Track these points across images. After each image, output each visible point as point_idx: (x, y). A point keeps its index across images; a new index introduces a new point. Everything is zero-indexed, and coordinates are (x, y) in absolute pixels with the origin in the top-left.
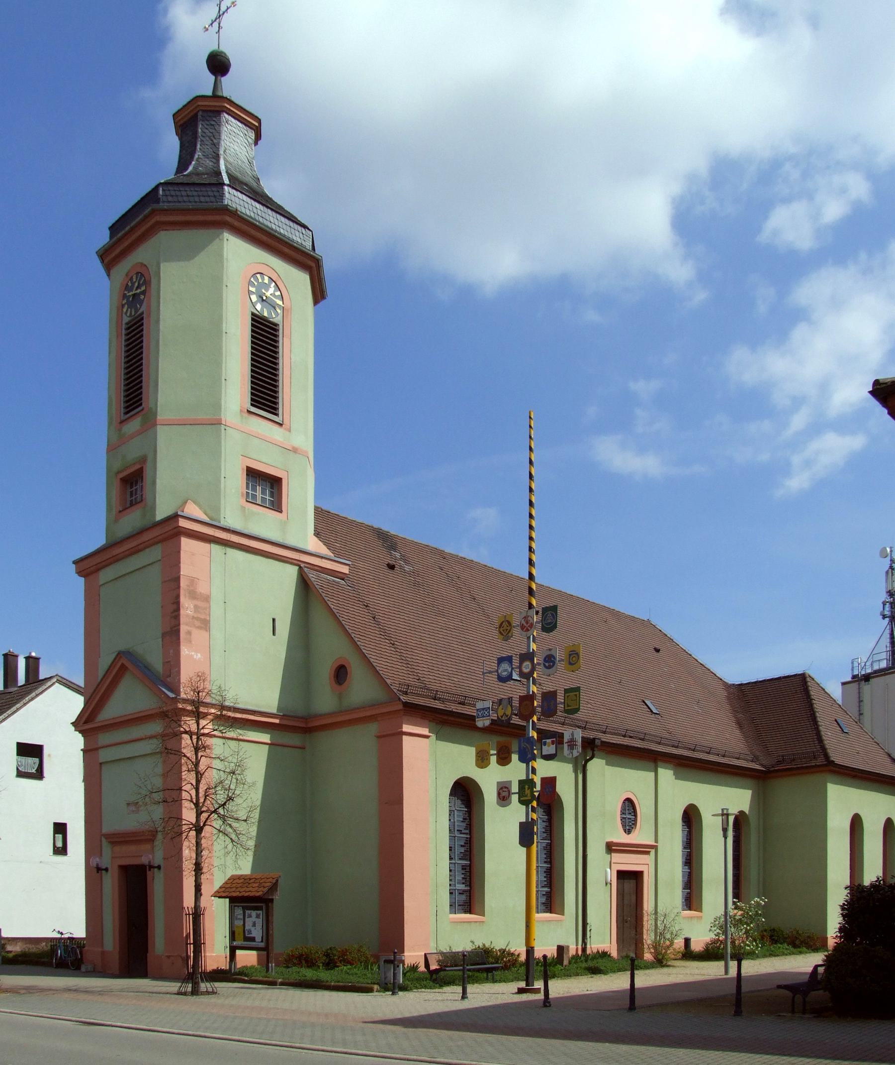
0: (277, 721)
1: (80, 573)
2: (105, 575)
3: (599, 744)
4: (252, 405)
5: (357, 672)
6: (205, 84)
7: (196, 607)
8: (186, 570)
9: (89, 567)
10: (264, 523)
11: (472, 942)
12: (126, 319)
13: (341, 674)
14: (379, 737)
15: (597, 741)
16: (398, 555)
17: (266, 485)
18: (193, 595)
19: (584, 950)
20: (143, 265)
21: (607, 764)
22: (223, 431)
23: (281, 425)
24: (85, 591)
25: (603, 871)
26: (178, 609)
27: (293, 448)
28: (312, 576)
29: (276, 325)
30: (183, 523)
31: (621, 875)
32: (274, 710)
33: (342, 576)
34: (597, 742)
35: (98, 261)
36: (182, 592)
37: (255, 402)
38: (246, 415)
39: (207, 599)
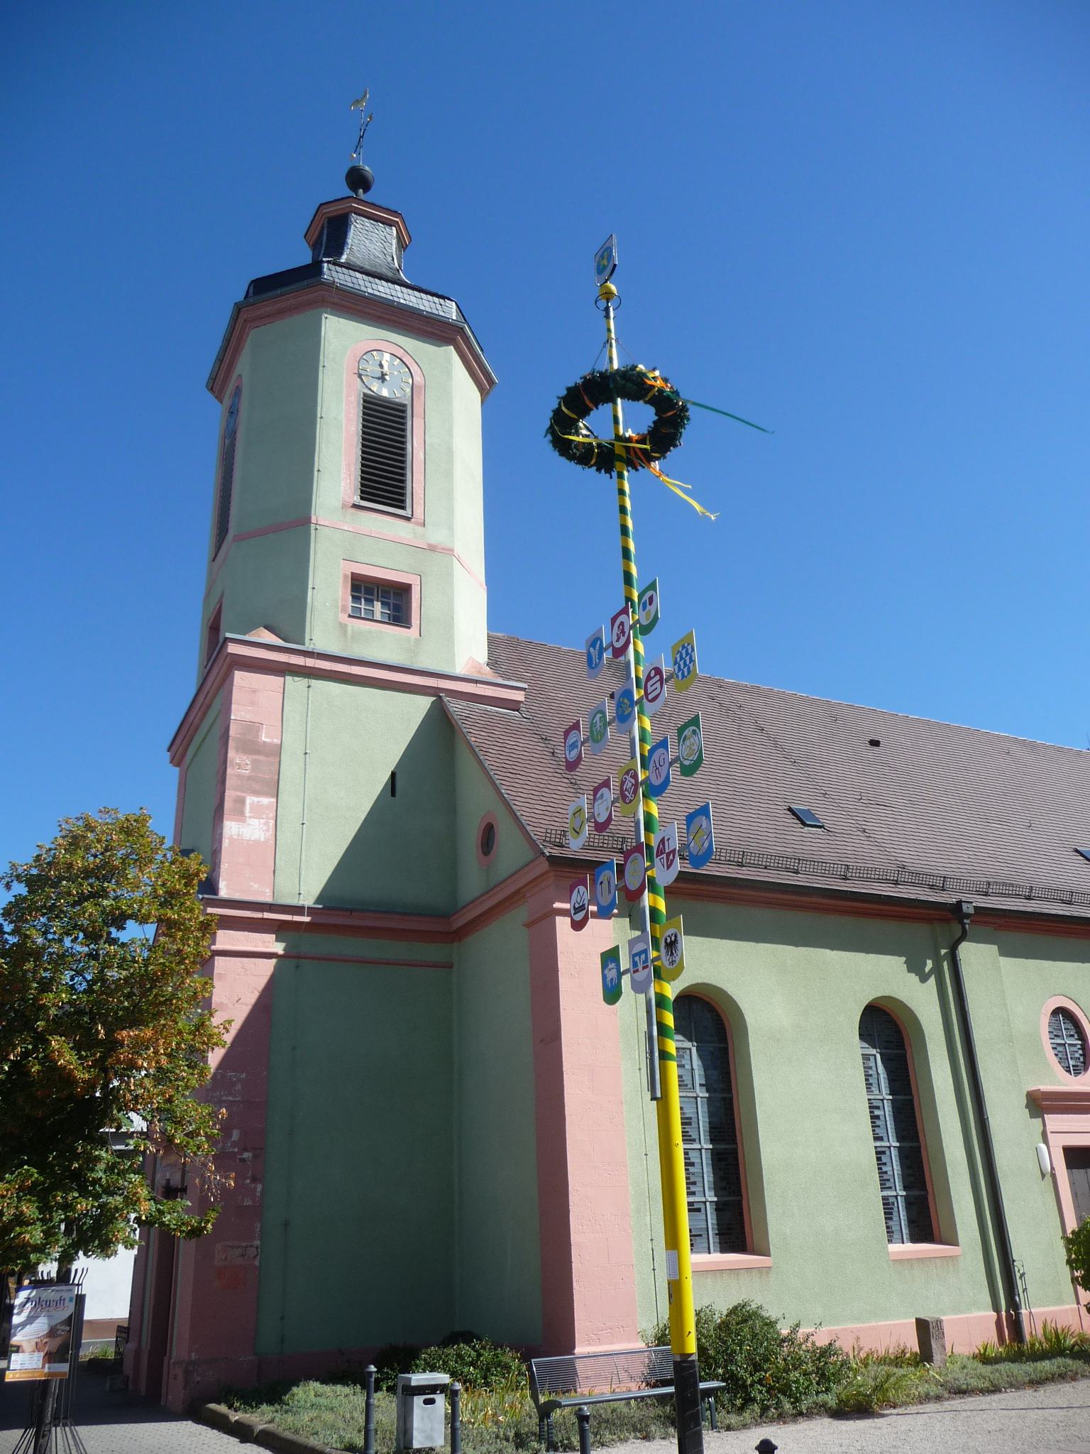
0: (307, 919)
3: (972, 911)
4: (362, 498)
7: (254, 762)
8: (239, 712)
10: (381, 642)
11: (923, 1327)
13: (488, 837)
15: (964, 906)
17: (388, 598)
18: (252, 747)
19: (368, 1397)
21: (1003, 953)
22: (313, 532)
23: (408, 519)
24: (365, 820)
27: (430, 545)
29: (405, 406)
30: (232, 649)
33: (514, 705)
35: (209, 394)
36: (231, 743)
38: (353, 510)
39: (276, 751)
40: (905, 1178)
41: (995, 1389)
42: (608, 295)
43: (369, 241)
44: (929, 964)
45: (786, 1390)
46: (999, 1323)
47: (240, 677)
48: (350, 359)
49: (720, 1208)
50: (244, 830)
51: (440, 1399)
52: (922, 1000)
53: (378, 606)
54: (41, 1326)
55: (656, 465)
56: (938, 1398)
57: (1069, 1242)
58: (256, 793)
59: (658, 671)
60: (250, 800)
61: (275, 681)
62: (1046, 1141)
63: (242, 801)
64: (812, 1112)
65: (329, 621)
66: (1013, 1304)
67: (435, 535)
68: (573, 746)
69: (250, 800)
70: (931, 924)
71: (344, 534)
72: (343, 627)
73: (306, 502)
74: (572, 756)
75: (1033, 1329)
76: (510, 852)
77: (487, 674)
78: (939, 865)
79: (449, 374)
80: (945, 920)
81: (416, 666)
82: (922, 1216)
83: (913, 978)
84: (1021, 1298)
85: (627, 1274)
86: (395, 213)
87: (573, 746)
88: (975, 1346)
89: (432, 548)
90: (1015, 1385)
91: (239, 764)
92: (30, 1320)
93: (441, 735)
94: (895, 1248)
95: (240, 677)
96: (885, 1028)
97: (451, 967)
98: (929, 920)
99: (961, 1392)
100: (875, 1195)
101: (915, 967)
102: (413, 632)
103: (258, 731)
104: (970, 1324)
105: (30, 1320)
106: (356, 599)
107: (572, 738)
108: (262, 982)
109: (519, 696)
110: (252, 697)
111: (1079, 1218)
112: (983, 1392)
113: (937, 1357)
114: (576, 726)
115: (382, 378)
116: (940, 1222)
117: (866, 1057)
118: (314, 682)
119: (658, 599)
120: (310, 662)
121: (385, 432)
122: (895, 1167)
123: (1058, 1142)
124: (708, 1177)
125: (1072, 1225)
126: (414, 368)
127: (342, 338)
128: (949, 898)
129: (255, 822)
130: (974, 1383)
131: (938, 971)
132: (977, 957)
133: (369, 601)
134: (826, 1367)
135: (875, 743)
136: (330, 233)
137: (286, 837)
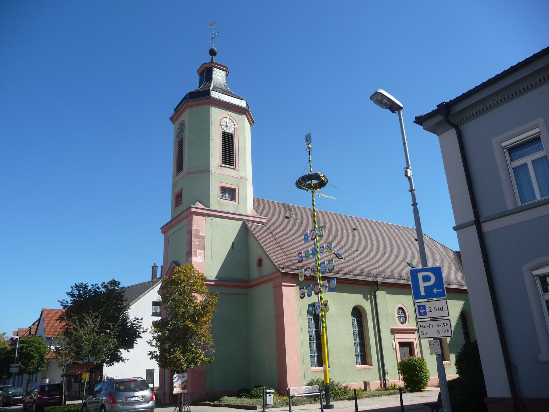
0: (214, 283)
1: (162, 232)
2: (170, 232)
5: (265, 262)
6: (208, 59)
8: (194, 227)
9: (165, 229)
10: (229, 206)
11: (365, 383)
12: (178, 139)
13: (260, 263)
14: (274, 288)
16: (291, 213)
17: (230, 193)
18: (198, 237)
20: (183, 121)
21: (387, 293)
25: (391, 343)
26: (191, 243)
28: (249, 224)
30: (193, 210)
31: (402, 345)
32: (213, 278)
33: (263, 223)
34: (379, 283)
36: (193, 236)
37: (224, 162)
39: (204, 238)
40: (360, 349)
41: (381, 396)
42: (309, 148)
43: (219, 76)
44: (369, 296)
45: (338, 395)
46: (381, 384)
47: (195, 218)
48: (220, 121)
49: (318, 357)
50: (197, 260)
51: (272, 395)
52: (367, 306)
53: (227, 194)
54: (180, 382)
55: (318, 190)
56: (369, 397)
57: (398, 364)
58: (200, 249)
59: (323, 247)
60: (198, 251)
61: (203, 218)
62: (394, 341)
63: (196, 252)
64: (340, 332)
65: (217, 201)
66: (385, 379)
67: (242, 174)
68: (300, 257)
69: (198, 251)
70: (370, 287)
71: (219, 175)
72: (219, 202)
73: (208, 165)
74: (300, 259)
75: (389, 385)
76: (267, 269)
77: (255, 214)
78: (372, 269)
79: (244, 124)
80: (373, 285)
81: (238, 213)
82: (364, 359)
83: (365, 300)
84: (386, 378)
85: (300, 372)
86: (225, 67)
87: (300, 257)
88: (376, 388)
89: (241, 178)
90: (386, 395)
91: (195, 241)
92: (178, 380)
93: (245, 231)
94: (358, 366)
95: (195, 218)
96: (358, 313)
97: (248, 295)
98: (369, 285)
99: (374, 396)
100: (354, 353)
101: (365, 297)
102: (236, 203)
103: (199, 232)
104: (375, 384)
105: (178, 380)
106: (221, 193)
107: (300, 255)
108: (455, 378)
109: (264, 221)
110: (198, 223)
111: (401, 359)
112: (378, 396)
113: (368, 390)
114: (301, 253)
115: (227, 126)
116: (368, 360)
117: (353, 320)
118: (213, 218)
119: (323, 230)
120: (212, 213)
121: (228, 140)
122: (358, 347)
123: (397, 341)
124: (315, 349)
125: (399, 360)
126: (235, 122)
127: (215, 113)
128: (375, 280)
129: (199, 257)
130: (376, 394)
131: (371, 298)
132: (381, 295)
133: (225, 193)
134: (345, 390)
135: (355, 229)
136: (206, 74)
137: (208, 261)
